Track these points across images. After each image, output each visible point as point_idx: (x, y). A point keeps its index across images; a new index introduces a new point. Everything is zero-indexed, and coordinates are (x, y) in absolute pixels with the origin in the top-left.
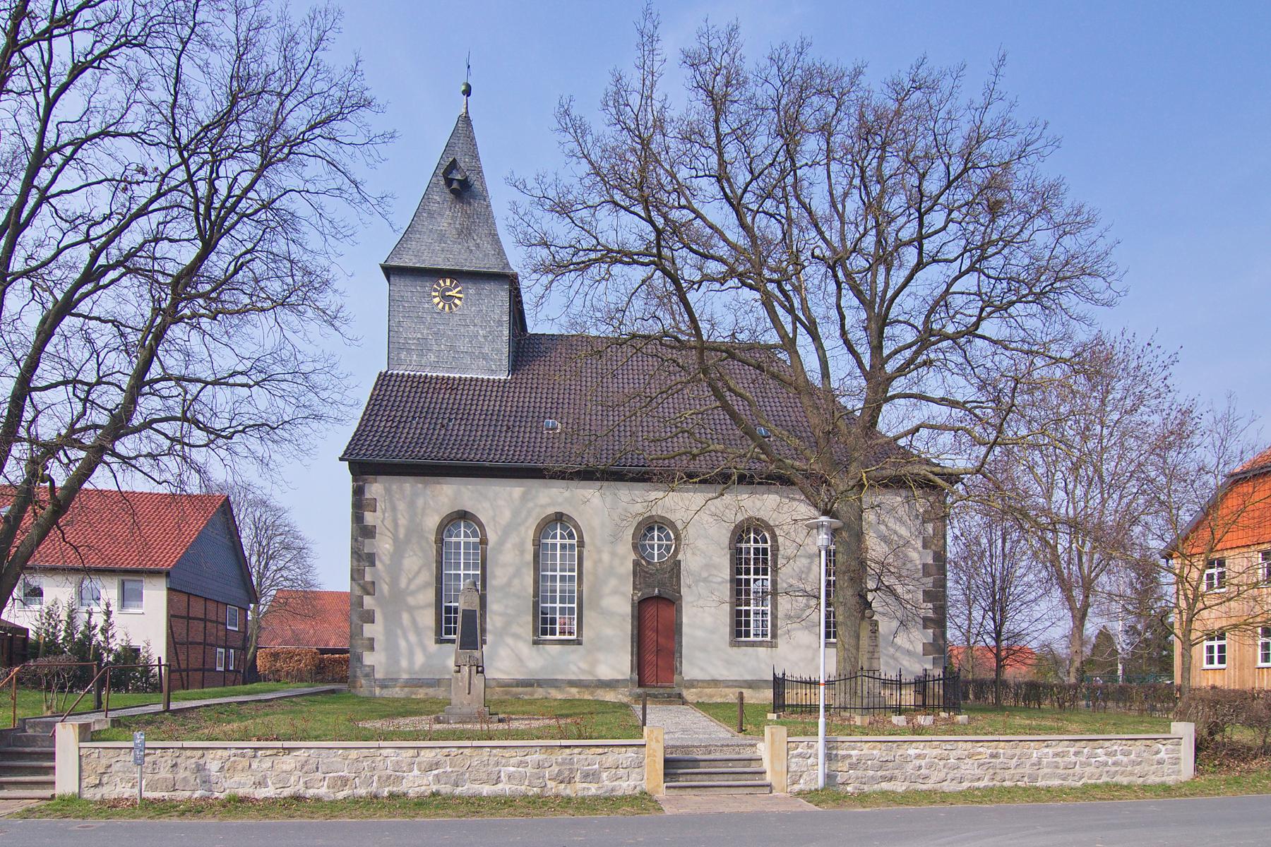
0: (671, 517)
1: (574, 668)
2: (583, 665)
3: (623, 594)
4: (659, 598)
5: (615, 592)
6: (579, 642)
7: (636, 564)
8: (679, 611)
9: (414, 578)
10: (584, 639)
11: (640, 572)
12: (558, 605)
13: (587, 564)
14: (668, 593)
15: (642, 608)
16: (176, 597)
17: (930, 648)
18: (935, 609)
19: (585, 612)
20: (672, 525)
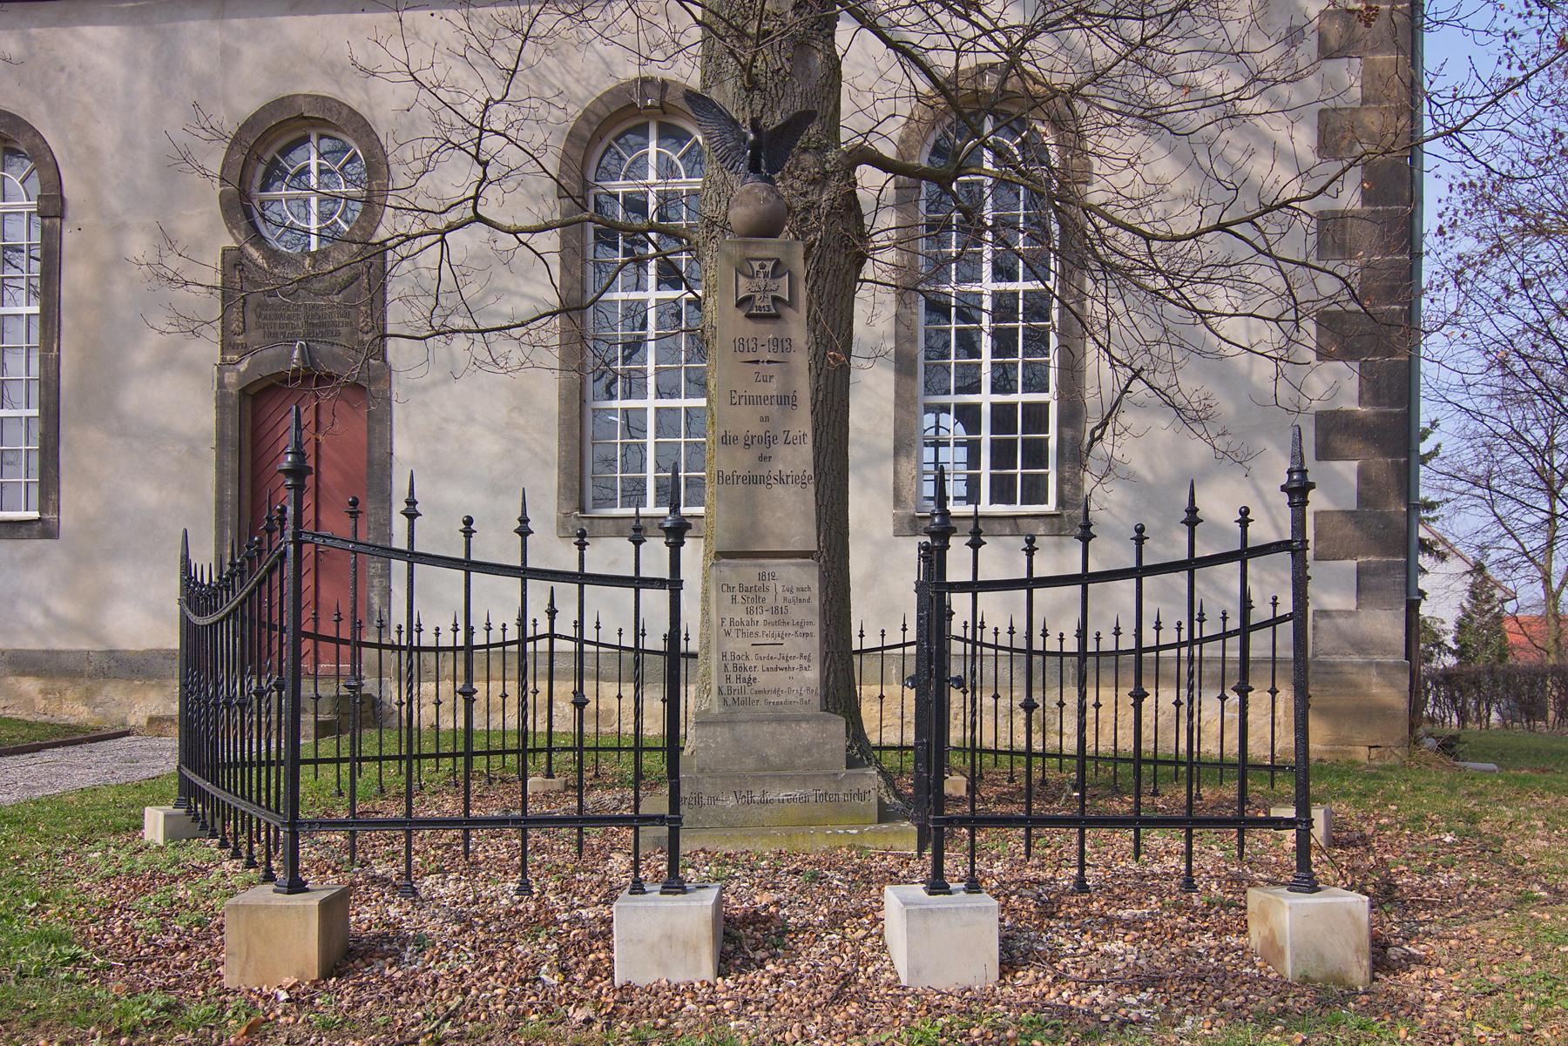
0: (353, 97)
1: (35, 617)
2: (64, 607)
3: (191, 368)
4: (312, 377)
5: (167, 362)
6: (45, 529)
7: (234, 262)
8: (380, 422)
9: (980, 27)
10: (67, 519)
11: (250, 292)
12: (651, 403)
13: (75, 276)
14: (337, 356)
15: (252, 410)
16: (639, 425)
17: (1349, 530)
18: (1371, 388)
19: (67, 431)
20: (362, 127)
